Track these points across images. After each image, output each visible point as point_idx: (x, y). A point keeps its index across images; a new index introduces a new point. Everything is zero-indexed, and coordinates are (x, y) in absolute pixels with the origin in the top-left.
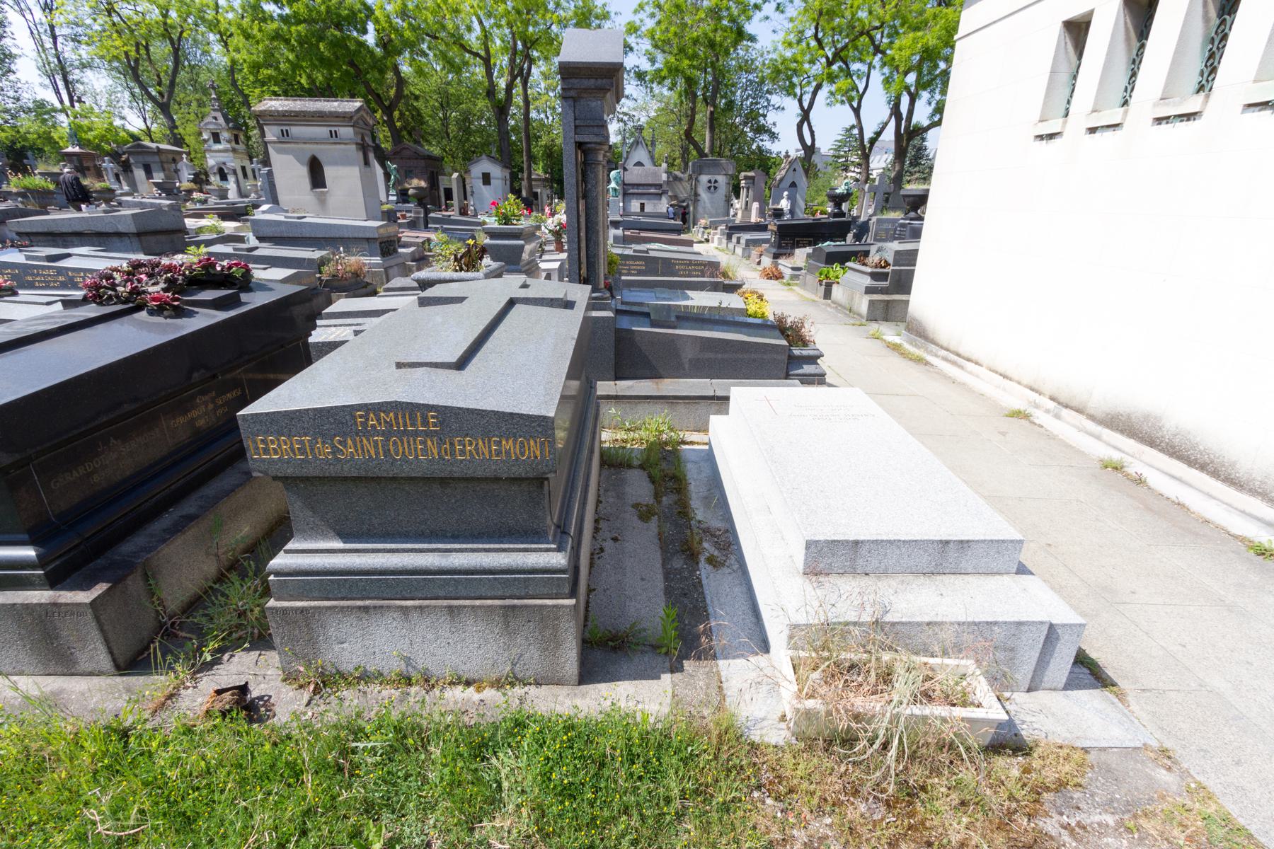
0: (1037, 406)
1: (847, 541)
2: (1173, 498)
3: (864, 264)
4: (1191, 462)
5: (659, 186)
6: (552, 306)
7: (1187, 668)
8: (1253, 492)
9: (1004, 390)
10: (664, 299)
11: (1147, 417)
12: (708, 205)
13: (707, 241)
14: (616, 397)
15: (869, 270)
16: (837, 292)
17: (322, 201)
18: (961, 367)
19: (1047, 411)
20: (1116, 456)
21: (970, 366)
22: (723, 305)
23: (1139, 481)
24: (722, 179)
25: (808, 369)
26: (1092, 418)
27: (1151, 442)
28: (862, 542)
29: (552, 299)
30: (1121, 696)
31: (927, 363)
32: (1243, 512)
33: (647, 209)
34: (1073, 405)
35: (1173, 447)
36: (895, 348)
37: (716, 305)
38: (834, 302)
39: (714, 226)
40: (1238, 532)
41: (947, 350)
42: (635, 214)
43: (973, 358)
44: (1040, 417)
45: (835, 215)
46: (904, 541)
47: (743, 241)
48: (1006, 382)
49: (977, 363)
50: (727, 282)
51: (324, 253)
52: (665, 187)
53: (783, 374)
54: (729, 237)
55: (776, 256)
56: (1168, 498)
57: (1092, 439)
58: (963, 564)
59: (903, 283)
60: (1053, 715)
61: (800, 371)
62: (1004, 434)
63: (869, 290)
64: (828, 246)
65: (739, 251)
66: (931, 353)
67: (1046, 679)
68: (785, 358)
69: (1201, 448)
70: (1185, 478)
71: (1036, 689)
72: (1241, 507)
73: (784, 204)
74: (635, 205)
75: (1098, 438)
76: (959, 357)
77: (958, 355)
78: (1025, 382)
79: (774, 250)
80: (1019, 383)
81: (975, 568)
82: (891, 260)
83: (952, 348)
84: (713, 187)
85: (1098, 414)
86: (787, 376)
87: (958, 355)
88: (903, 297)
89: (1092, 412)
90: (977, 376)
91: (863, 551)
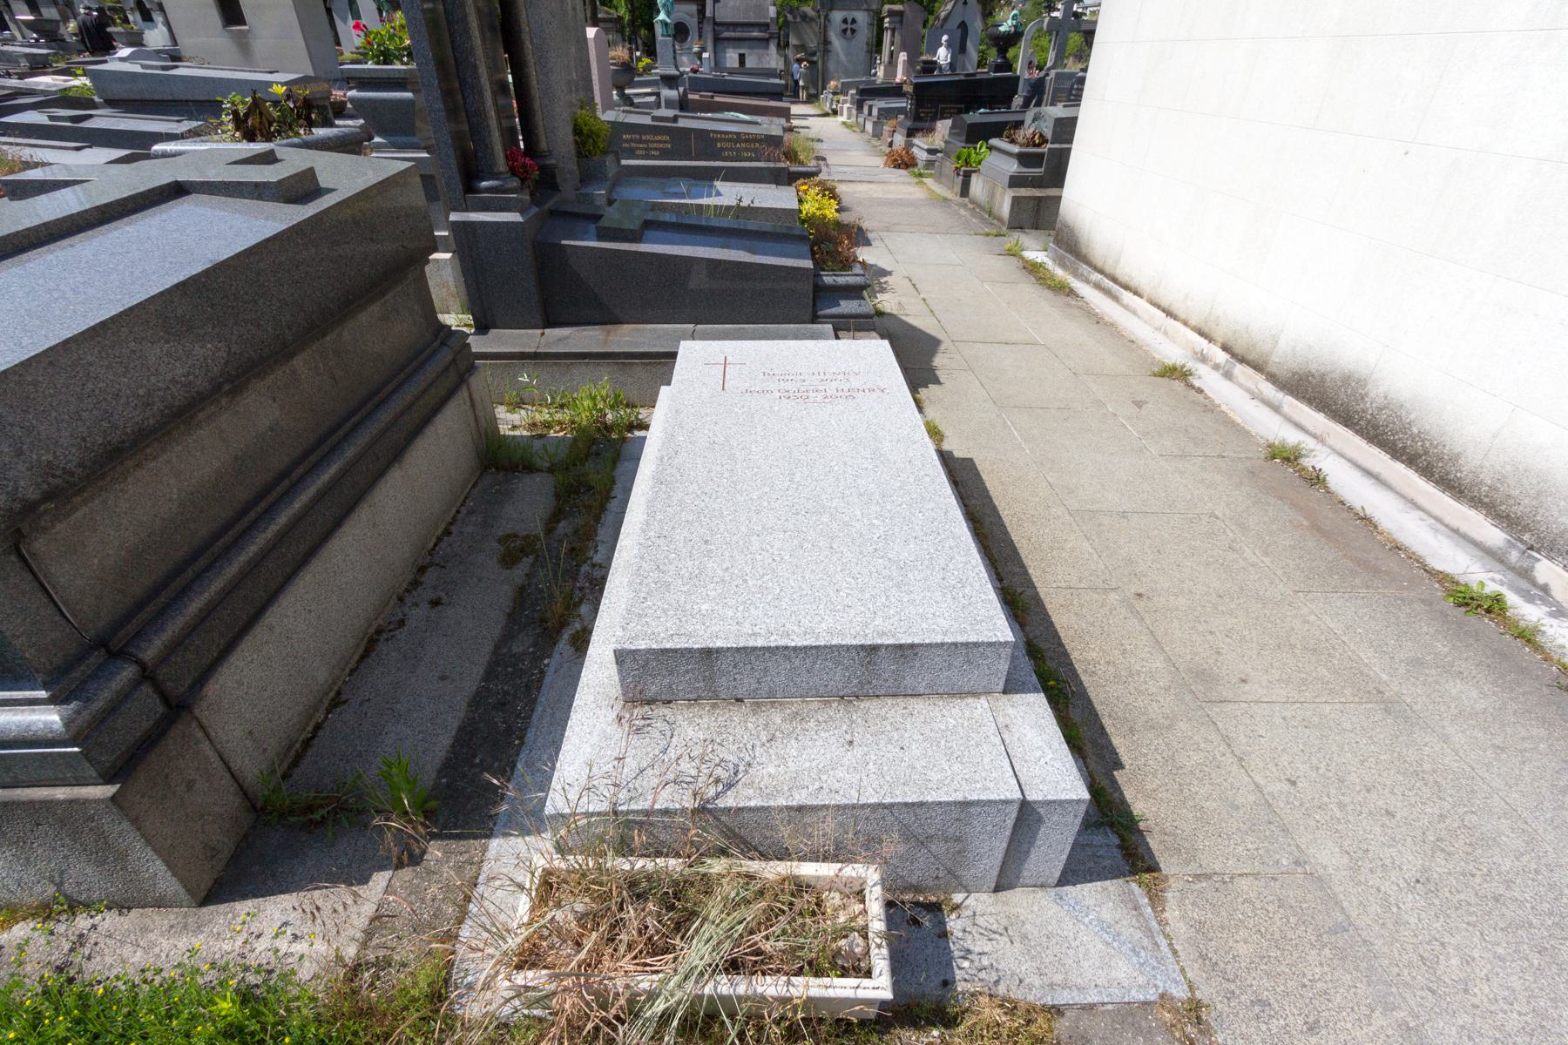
0: (1203, 359)
1: (690, 650)
2: (1357, 506)
3: (1013, 141)
4: (1398, 452)
5: (764, 26)
6: (259, 198)
7: (1285, 830)
8: (1476, 502)
9: (1166, 333)
10: (676, 195)
11: (1347, 379)
12: (843, 57)
13: (835, 113)
14: (535, 356)
15: (1016, 149)
16: (977, 186)
17: (244, 47)
18: (1116, 298)
19: (1216, 367)
20: (1292, 437)
21: (1127, 296)
22: (745, 203)
23: (1316, 480)
24: (861, 17)
25: (847, 306)
26: (1272, 378)
27: (1346, 417)
28: (719, 650)
29: (257, 185)
30: (1156, 899)
31: (1071, 293)
32: (1456, 531)
33: (750, 63)
34: (1251, 358)
35: (1375, 427)
36: (1033, 269)
37: (734, 203)
38: (972, 202)
39: (843, 91)
40: (1439, 566)
41: (1101, 272)
42: (732, 72)
43: (1132, 284)
44: (1207, 379)
45: (998, 68)
46: (795, 649)
47: (875, 112)
48: (1171, 321)
49: (1136, 293)
50: (795, 168)
51: (195, 124)
52: (774, 29)
53: (808, 316)
54: (860, 108)
55: (911, 133)
56: (1350, 508)
57: (1266, 410)
58: (909, 681)
59: (1056, 171)
60: (1025, 937)
61: (834, 311)
62: (1139, 404)
63: (1015, 182)
64: (979, 116)
65: (869, 127)
66: (1076, 274)
67: (1025, 873)
68: (809, 288)
69: (1415, 430)
70: (1385, 475)
71: (1010, 887)
72: (1454, 524)
73: (943, 55)
74: (731, 57)
75: (1276, 408)
76: (1116, 284)
77: (1114, 280)
78: (1193, 322)
79: (909, 123)
80: (1185, 323)
81: (929, 686)
82: (1048, 134)
83: (1108, 269)
84: (849, 30)
85: (1282, 373)
86: (815, 319)
87: (1114, 280)
88: (1052, 192)
89: (1273, 369)
90: (1134, 313)
91: (724, 664)
